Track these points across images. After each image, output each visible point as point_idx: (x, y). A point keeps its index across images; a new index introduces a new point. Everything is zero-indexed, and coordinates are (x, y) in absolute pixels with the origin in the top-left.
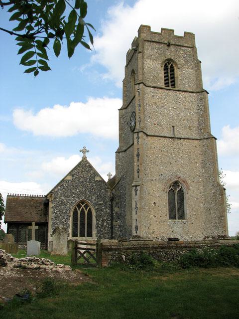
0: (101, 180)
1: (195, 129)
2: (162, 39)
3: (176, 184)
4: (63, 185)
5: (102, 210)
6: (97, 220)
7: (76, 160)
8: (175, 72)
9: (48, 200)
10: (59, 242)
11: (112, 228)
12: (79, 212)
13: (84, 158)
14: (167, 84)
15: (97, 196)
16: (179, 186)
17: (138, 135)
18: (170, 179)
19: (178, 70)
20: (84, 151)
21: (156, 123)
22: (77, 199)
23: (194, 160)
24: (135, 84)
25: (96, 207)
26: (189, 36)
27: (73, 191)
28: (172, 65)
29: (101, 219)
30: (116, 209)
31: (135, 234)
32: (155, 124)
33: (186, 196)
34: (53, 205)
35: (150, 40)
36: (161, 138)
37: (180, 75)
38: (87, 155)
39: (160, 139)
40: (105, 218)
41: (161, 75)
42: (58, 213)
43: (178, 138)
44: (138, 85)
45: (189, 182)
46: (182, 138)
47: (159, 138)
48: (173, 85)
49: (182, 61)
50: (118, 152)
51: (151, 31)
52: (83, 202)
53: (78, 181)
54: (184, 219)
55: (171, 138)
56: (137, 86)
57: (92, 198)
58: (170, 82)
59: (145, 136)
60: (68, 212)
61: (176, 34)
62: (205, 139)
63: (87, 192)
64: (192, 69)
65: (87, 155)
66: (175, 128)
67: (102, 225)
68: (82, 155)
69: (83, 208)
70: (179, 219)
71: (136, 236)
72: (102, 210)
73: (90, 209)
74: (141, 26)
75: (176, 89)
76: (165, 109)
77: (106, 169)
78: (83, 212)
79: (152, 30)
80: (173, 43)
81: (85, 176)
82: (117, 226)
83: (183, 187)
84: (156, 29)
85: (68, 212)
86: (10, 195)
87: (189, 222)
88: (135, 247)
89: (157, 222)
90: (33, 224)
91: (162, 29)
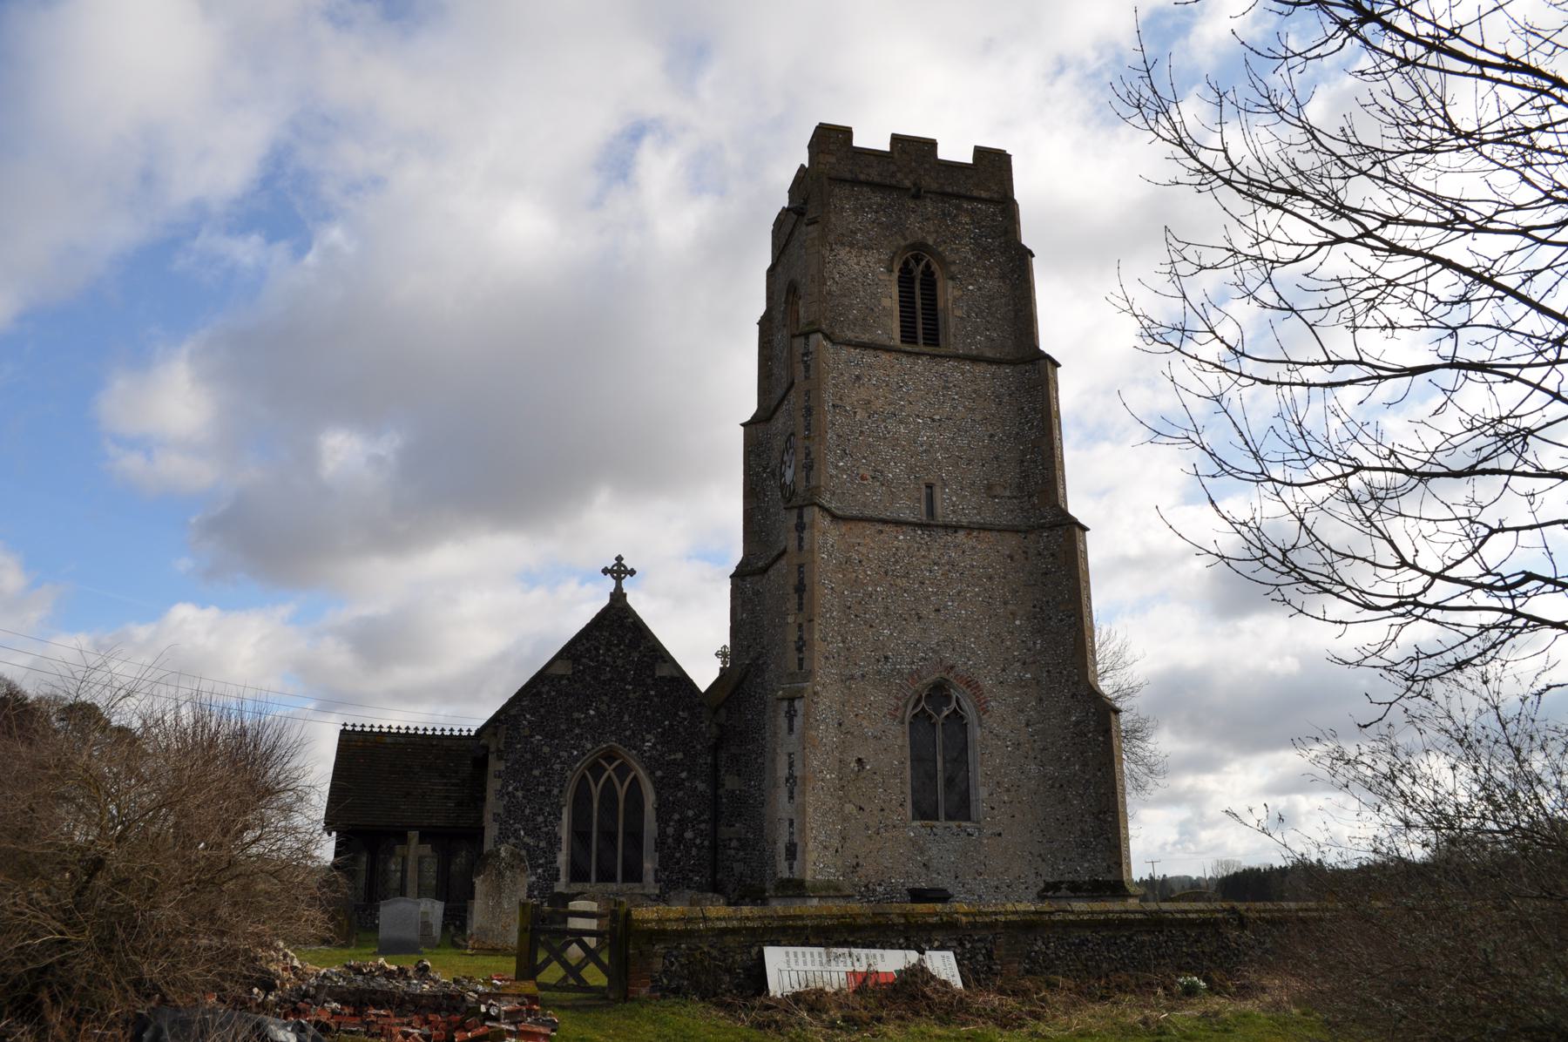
0: (676, 674)
1: (1008, 493)
2: (893, 175)
3: (939, 692)
4: (539, 693)
5: (679, 785)
6: (659, 818)
7: (589, 604)
8: (940, 292)
9: (486, 748)
10: (499, 903)
11: (714, 847)
12: (596, 793)
13: (618, 596)
14: (908, 335)
15: (663, 734)
16: (948, 698)
17: (800, 516)
18: (915, 675)
19: (950, 283)
20: (619, 571)
21: (868, 474)
22: (589, 746)
23: (1006, 603)
24: (793, 336)
25: (659, 773)
26: (993, 166)
27: (576, 715)
28: (928, 266)
29: (676, 817)
30: (731, 782)
31: (786, 875)
32: (863, 478)
33: (976, 734)
34: (501, 766)
35: (848, 176)
36: (886, 528)
37: (956, 300)
38: (628, 584)
39: (881, 532)
40: (690, 813)
41: (886, 302)
42: (520, 794)
43: (946, 527)
44: (802, 340)
45: (987, 683)
46: (962, 527)
47: (880, 527)
48: (933, 338)
49: (966, 252)
50: (738, 577)
51: (855, 144)
52: (610, 756)
53: (595, 678)
54: (968, 819)
55: (921, 526)
56: (799, 343)
57: (644, 741)
58: (920, 326)
59: (828, 519)
60: (556, 791)
61: (943, 154)
62: (1042, 527)
63: (626, 718)
64: (1003, 277)
65: (628, 584)
66: (937, 490)
67: (679, 838)
68: (610, 584)
69: (609, 777)
70: (949, 817)
71: (789, 880)
72: (679, 785)
73: (635, 778)
74: (1009, 156)
75: (942, 350)
76: (901, 422)
77: (697, 638)
78: (609, 793)
79: (858, 142)
80: (934, 186)
81: (619, 662)
82: (734, 844)
83: (963, 704)
84: (872, 136)
85: (556, 791)
86: (349, 728)
87: (987, 831)
88: (749, 924)
89: (867, 828)
90: (414, 835)
91: (896, 139)
